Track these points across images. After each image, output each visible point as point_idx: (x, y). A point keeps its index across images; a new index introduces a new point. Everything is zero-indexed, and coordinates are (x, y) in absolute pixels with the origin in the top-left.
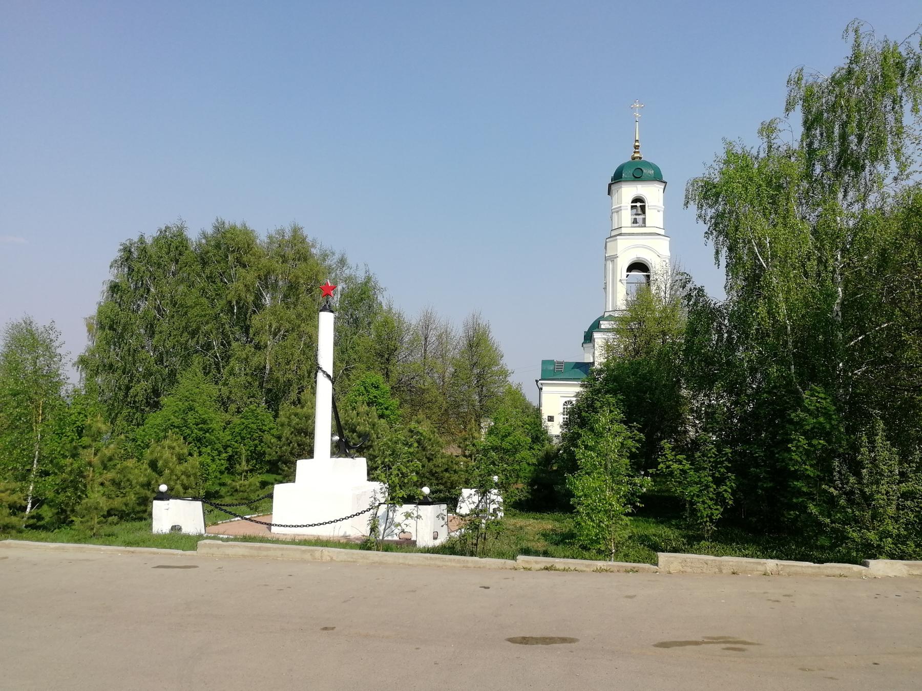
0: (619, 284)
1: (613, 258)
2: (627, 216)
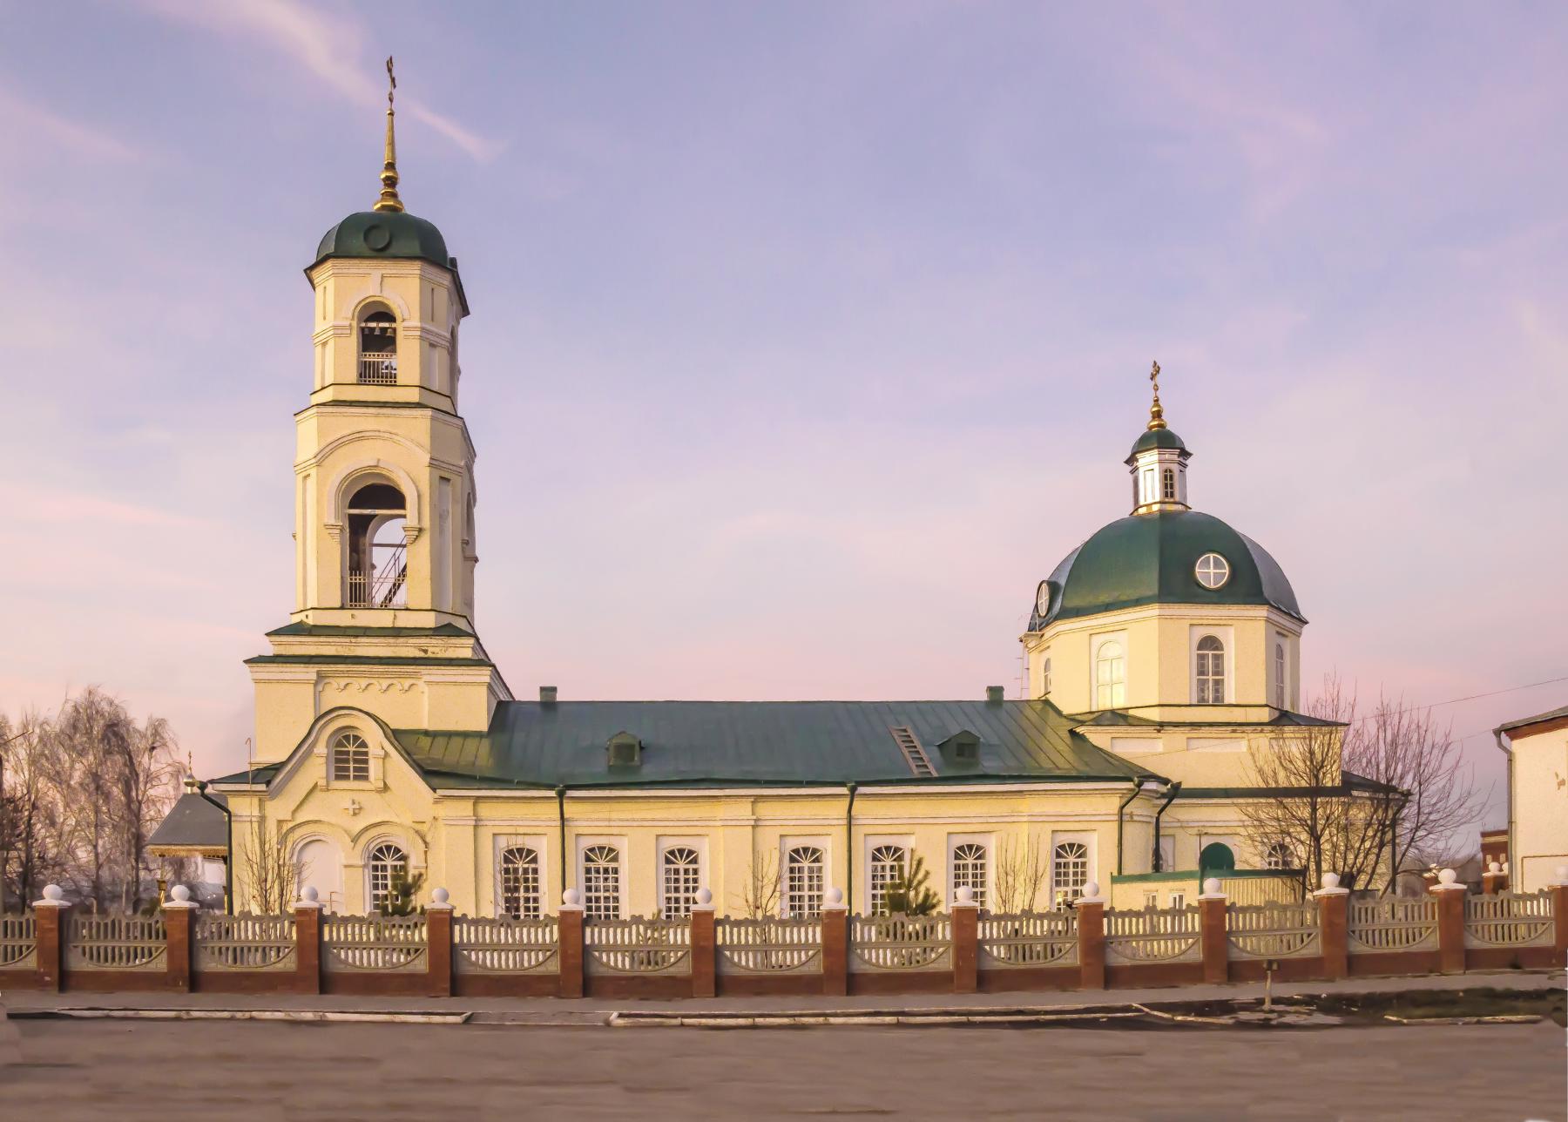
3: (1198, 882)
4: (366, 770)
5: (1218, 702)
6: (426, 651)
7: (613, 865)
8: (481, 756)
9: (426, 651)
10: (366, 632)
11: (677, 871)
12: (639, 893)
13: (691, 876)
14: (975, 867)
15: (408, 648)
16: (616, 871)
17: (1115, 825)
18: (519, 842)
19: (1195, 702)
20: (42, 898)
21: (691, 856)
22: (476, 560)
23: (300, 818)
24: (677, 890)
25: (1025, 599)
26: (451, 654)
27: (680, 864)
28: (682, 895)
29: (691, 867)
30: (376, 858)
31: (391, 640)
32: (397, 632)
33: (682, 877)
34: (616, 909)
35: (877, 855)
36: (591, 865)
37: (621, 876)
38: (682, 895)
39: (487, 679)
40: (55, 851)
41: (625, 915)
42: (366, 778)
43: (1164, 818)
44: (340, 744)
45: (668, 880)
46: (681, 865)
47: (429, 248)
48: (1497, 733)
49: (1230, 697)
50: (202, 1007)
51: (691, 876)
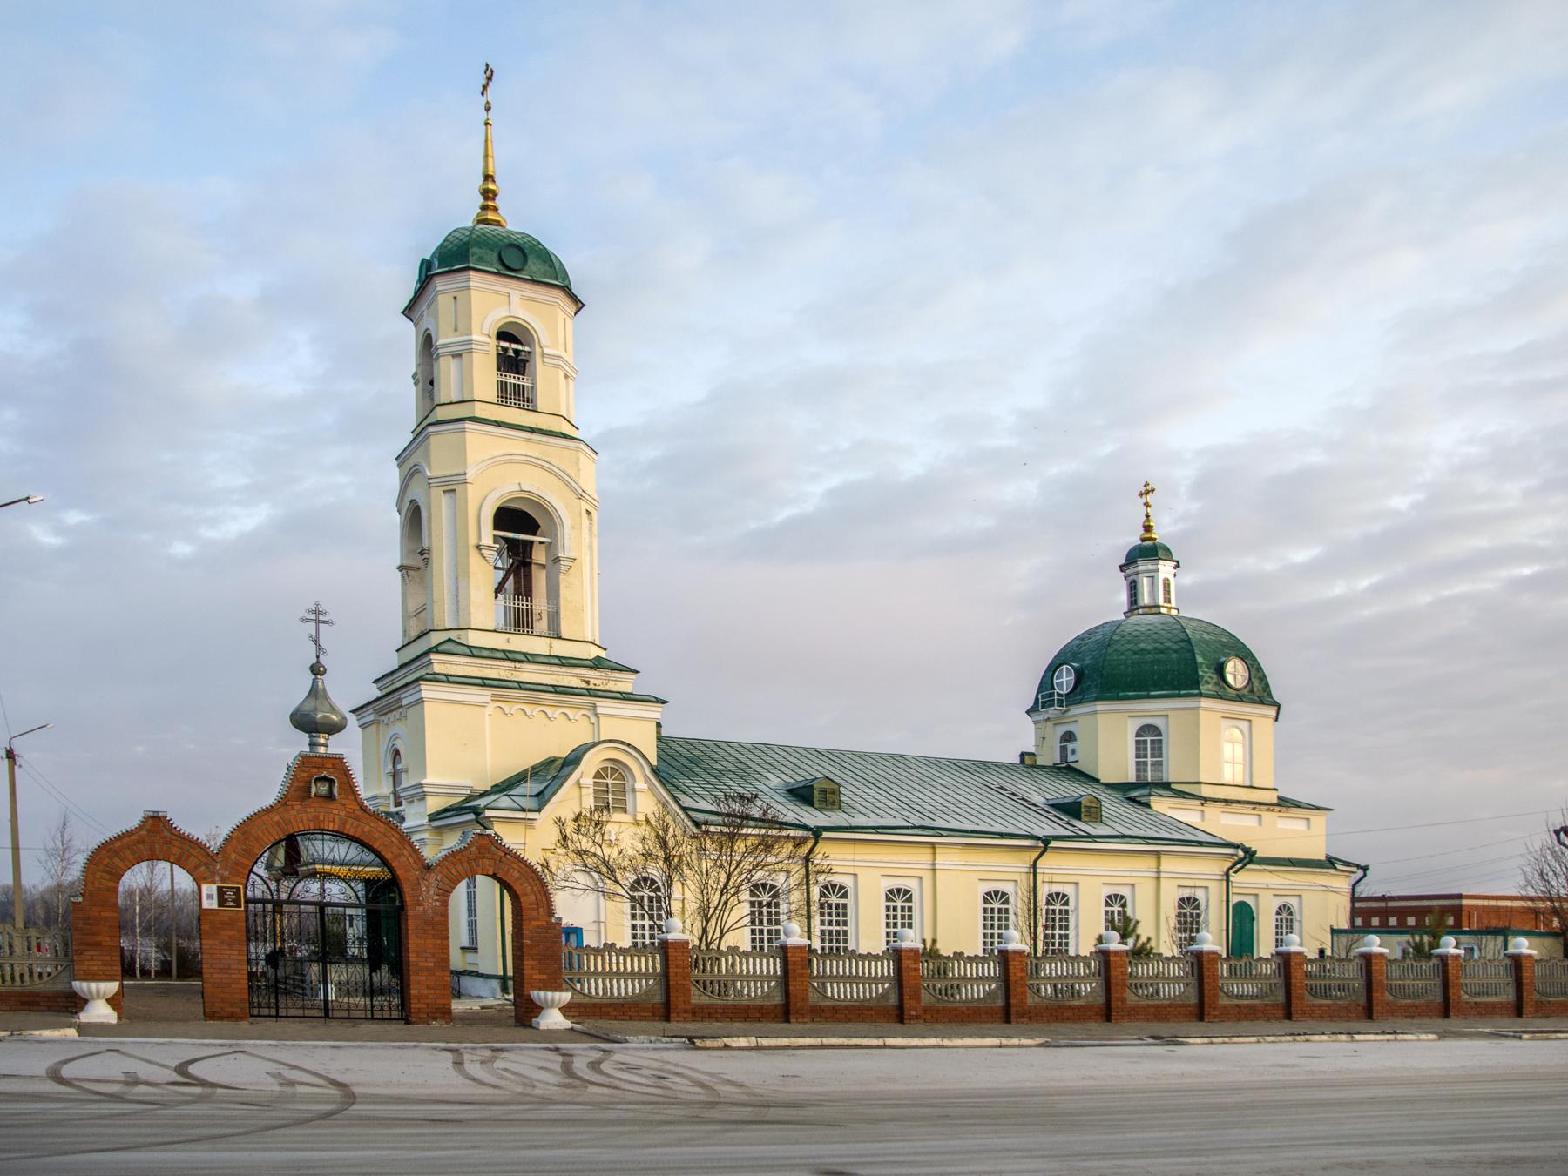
0: (474, 557)
1: (454, 485)
2: (484, 377)
3: (176, 887)
6: (588, 683)
7: (843, 901)
9: (588, 683)
10: (529, 658)
11: (760, 903)
14: (1000, 910)
15: (571, 678)
18: (1056, 888)
22: (401, 568)
24: (992, 926)
26: (612, 686)
27: (899, 903)
28: (996, 931)
31: (555, 669)
32: (564, 662)
33: (899, 913)
34: (846, 941)
35: (891, 894)
38: (996, 931)
40: (209, 889)
41: (1072, 953)
43: (1039, 864)
45: (845, 915)
47: (519, 259)
48: (1557, 833)
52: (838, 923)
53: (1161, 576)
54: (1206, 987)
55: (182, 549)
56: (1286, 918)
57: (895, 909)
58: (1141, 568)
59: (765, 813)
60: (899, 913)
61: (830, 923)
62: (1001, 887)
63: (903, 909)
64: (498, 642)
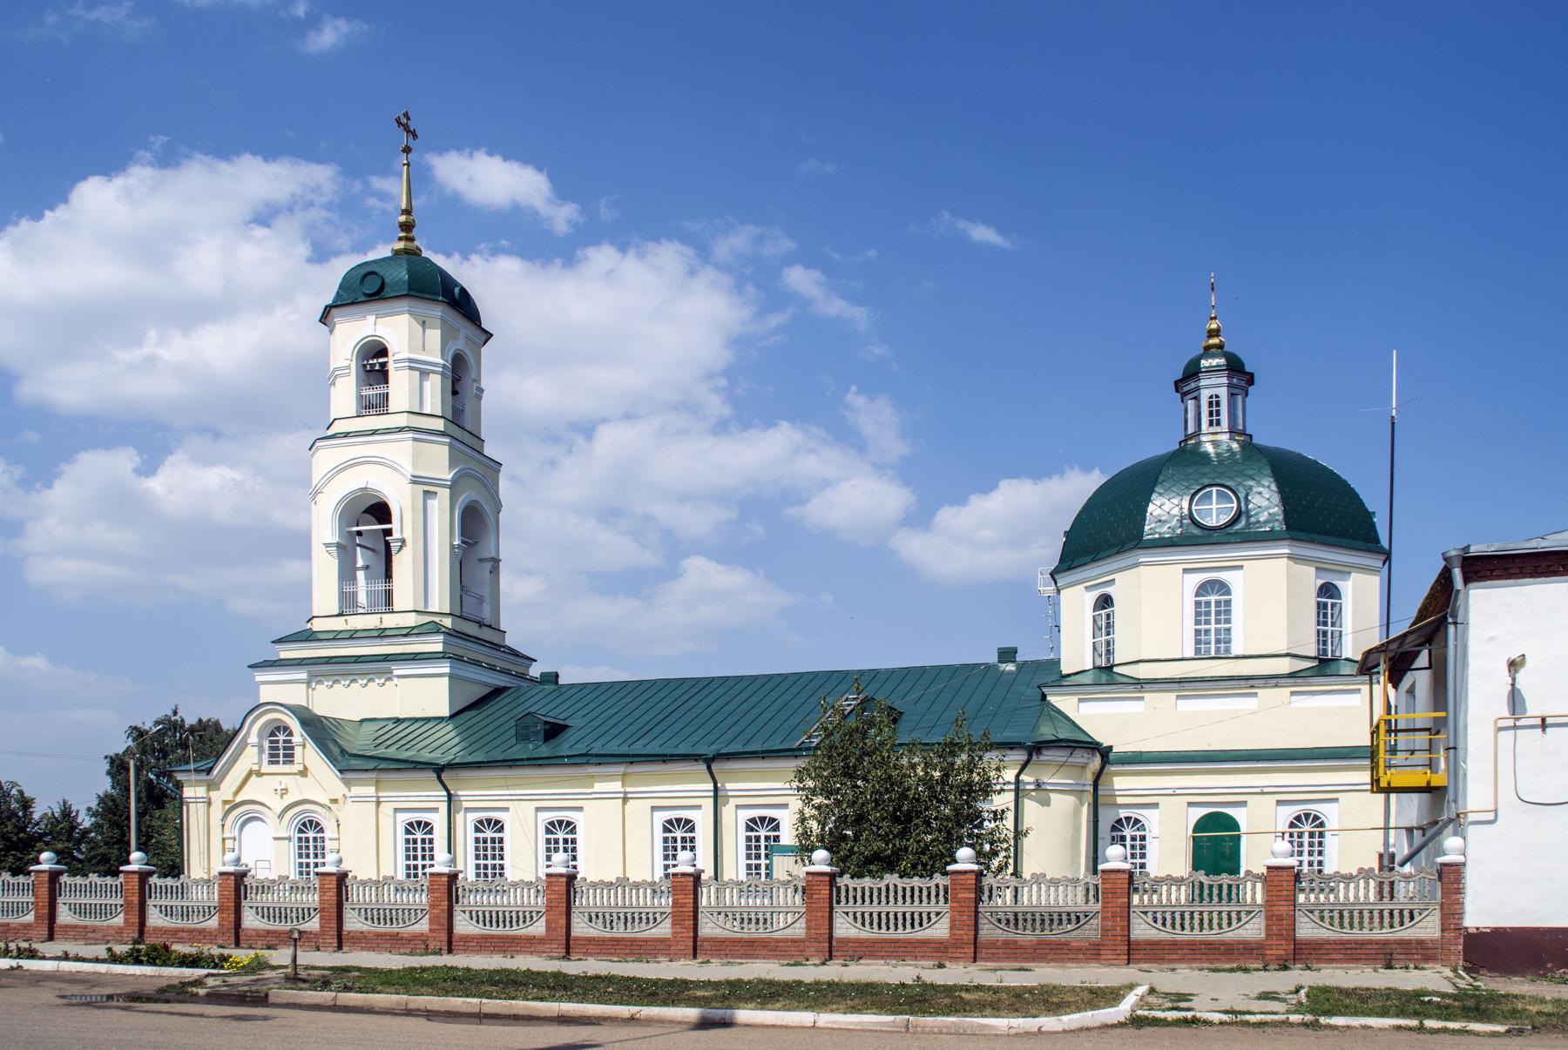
4: (292, 755)
5: (1224, 655)
8: (447, 743)
11: (307, 840)
12: (525, 861)
13: (1316, 840)
14: (315, 839)
16: (501, 840)
17: (711, 801)
19: (1190, 653)
20: (128, 862)
21: (498, 825)
23: (239, 799)
24: (415, 858)
25: (1052, 550)
28: (420, 862)
29: (570, 836)
30: (301, 831)
33: (419, 846)
35: (752, 824)
36: (481, 835)
37: (506, 845)
38: (420, 862)
39: (447, 670)
42: (292, 762)
44: (273, 734)
46: (311, 834)
49: (1236, 649)
50: (1421, 1036)
51: (1316, 848)
52: (494, 858)
53: (1205, 395)
54: (232, 917)
55: (1235, 446)
56: (1308, 828)
57: (415, 842)
58: (1203, 383)
59: (826, 729)
60: (419, 846)
61: (486, 857)
62: (424, 817)
63: (423, 841)
64: (338, 624)
